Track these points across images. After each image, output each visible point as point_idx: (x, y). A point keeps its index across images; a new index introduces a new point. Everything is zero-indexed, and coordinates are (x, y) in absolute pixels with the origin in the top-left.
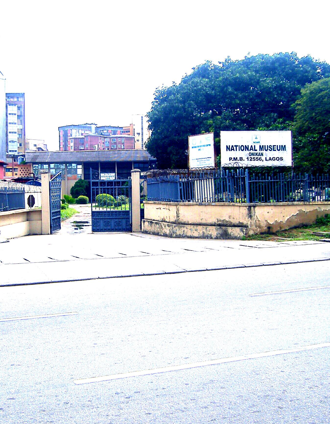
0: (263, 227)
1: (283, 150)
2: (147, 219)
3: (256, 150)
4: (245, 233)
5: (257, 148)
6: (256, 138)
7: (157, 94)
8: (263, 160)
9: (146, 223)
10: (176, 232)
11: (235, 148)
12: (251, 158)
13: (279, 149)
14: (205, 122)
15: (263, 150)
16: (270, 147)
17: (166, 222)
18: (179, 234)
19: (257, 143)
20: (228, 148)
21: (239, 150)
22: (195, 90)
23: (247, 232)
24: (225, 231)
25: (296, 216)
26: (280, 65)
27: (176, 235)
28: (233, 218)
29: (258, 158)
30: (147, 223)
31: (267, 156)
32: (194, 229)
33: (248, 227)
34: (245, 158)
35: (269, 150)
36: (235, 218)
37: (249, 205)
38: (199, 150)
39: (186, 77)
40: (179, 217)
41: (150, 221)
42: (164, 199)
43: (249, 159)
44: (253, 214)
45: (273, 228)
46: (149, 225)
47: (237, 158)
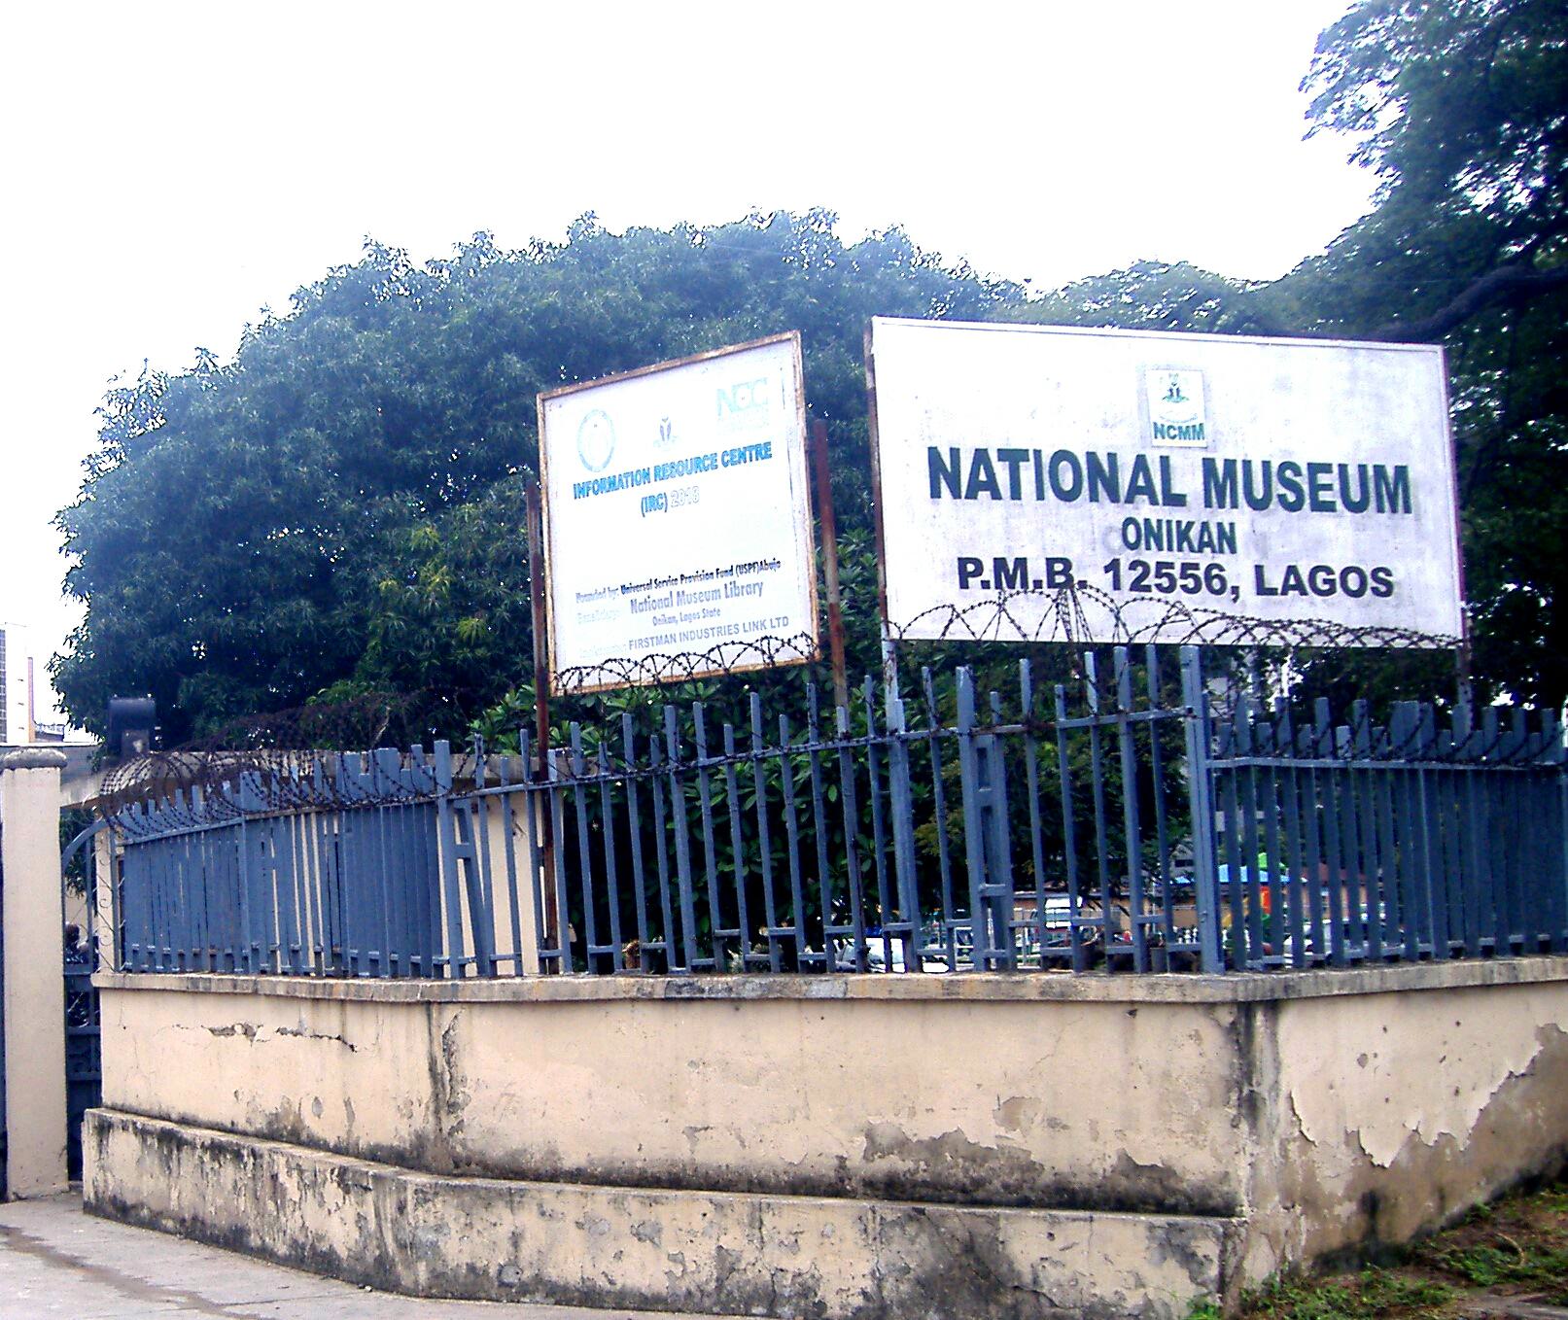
0: (1332, 1201)
1: (1387, 505)
2: (122, 1110)
3: (1178, 501)
4: (1213, 1272)
5: (1189, 481)
6: (1174, 394)
7: (113, 410)
8: (1235, 590)
9: (124, 1145)
10: (434, 1245)
11: (1002, 472)
12: (1140, 570)
13: (1355, 495)
14: (390, 535)
15: (1234, 505)
16: (1289, 474)
17: (314, 1144)
18: (471, 1268)
19: (1184, 433)
20: (942, 473)
21: (1040, 496)
22: (332, 376)
23: (1232, 1261)
24: (969, 1248)
25: (1528, 1080)
26: (755, 274)
27: (436, 1276)
28: (1053, 1124)
29: (1201, 573)
30: (134, 1141)
31: (1265, 554)
32: (624, 1225)
33: (1227, 1209)
34: (1090, 571)
35: (1282, 498)
36: (1080, 1129)
37: (1241, 999)
38: (651, 504)
39: (266, 327)
40: (453, 1107)
41: (160, 1124)
42: (159, 959)
43: (1128, 577)
44: (1268, 1079)
45: (1395, 1206)
46: (152, 1162)
47: (1021, 563)
